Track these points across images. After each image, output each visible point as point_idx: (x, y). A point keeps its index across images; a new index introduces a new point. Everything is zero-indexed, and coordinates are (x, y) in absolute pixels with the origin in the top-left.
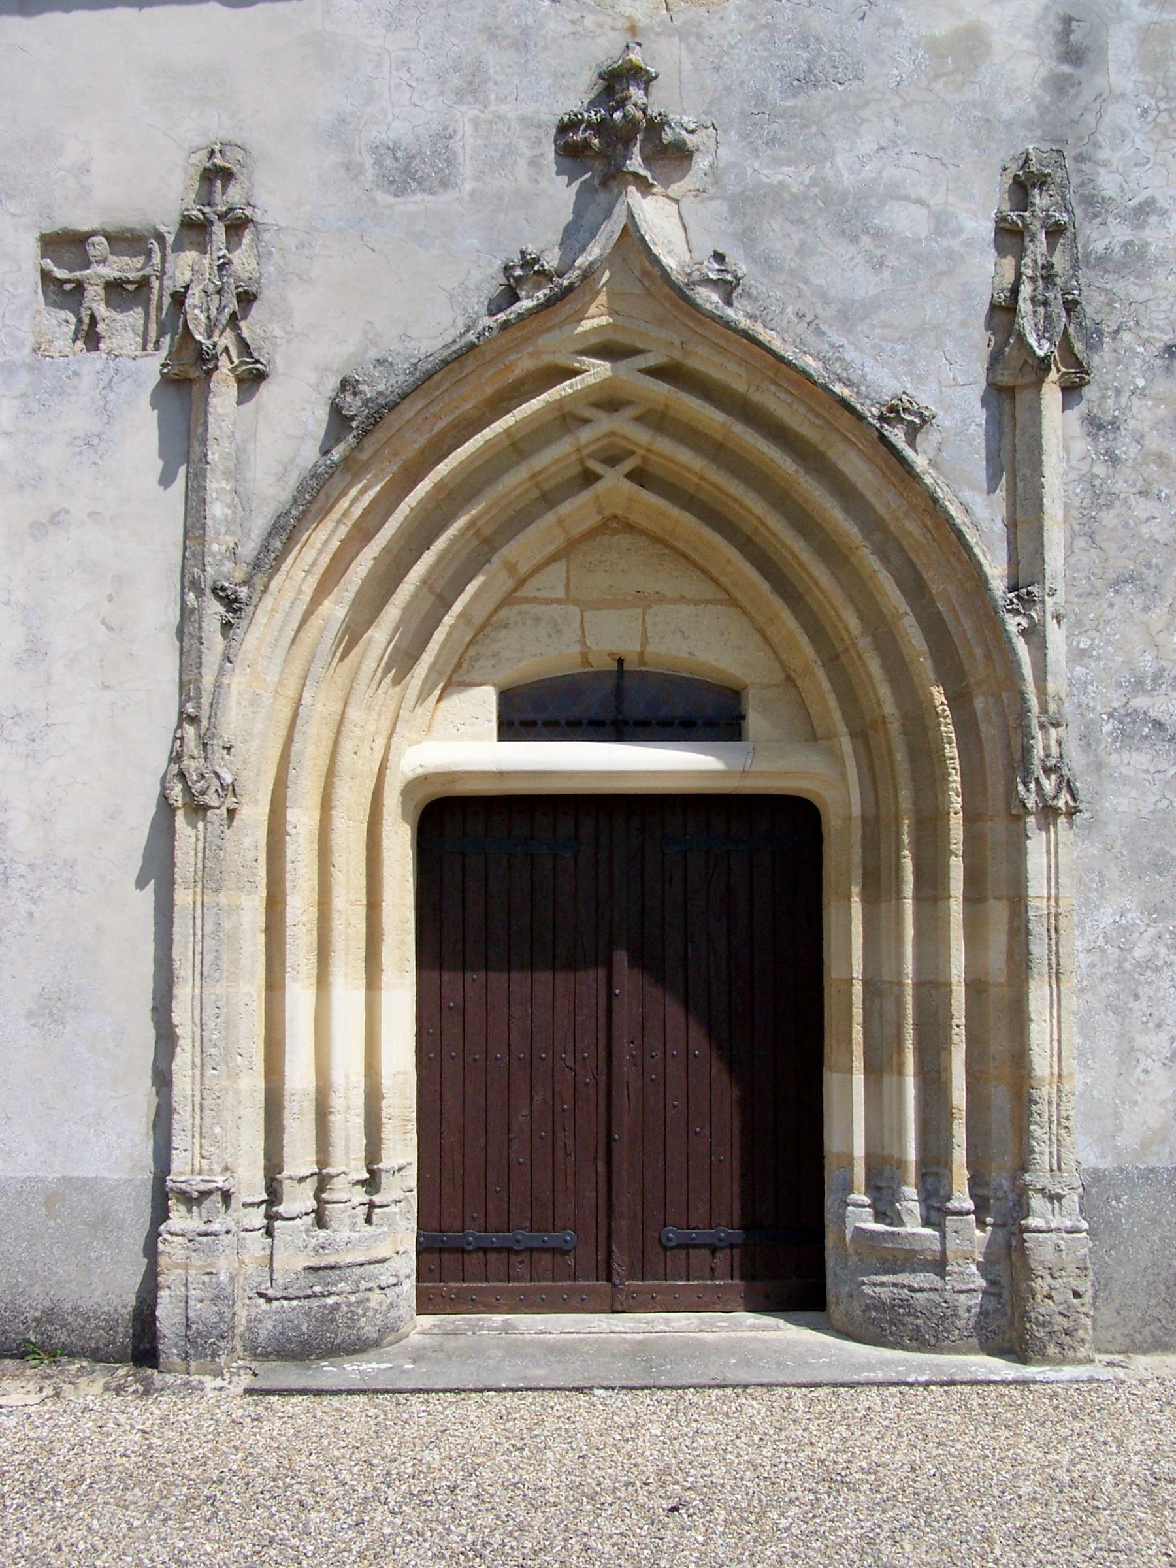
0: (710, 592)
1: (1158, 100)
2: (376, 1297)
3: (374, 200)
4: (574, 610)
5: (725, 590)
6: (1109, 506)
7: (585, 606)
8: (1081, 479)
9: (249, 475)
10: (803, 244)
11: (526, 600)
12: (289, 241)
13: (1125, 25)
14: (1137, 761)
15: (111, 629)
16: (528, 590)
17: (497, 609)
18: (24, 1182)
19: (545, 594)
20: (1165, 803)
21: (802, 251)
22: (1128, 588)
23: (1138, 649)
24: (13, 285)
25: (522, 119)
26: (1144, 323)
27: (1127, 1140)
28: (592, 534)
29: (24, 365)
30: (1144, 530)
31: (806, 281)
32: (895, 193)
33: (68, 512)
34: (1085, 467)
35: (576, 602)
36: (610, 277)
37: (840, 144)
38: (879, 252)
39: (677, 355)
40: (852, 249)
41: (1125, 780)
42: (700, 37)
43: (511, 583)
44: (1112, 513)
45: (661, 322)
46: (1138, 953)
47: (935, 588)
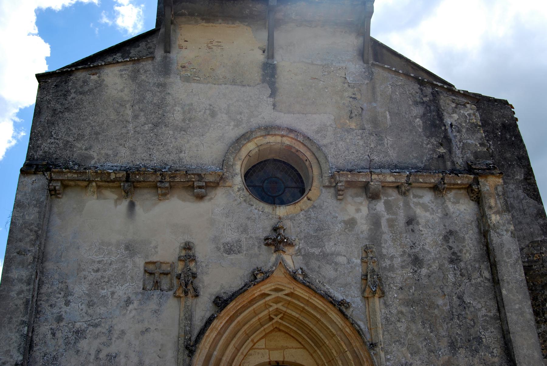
0: (299, 345)
1: (393, 234)
3: (223, 256)
5: (302, 345)
6: (391, 324)
7: (270, 350)
8: (384, 318)
9: (194, 320)
10: (319, 265)
12: (204, 265)
13: (384, 218)
15: (159, 357)
16: (256, 346)
17: (249, 351)
21: (319, 267)
22: (397, 343)
23: (401, 358)
24: (138, 274)
25: (256, 237)
26: (395, 282)
29: (140, 293)
30: (400, 329)
31: (321, 274)
32: (339, 254)
33: (150, 328)
35: (268, 349)
37: (326, 243)
38: (336, 267)
39: (292, 291)
40: (331, 267)
43: (252, 344)
44: (392, 325)
45: (289, 283)
47: (354, 344)
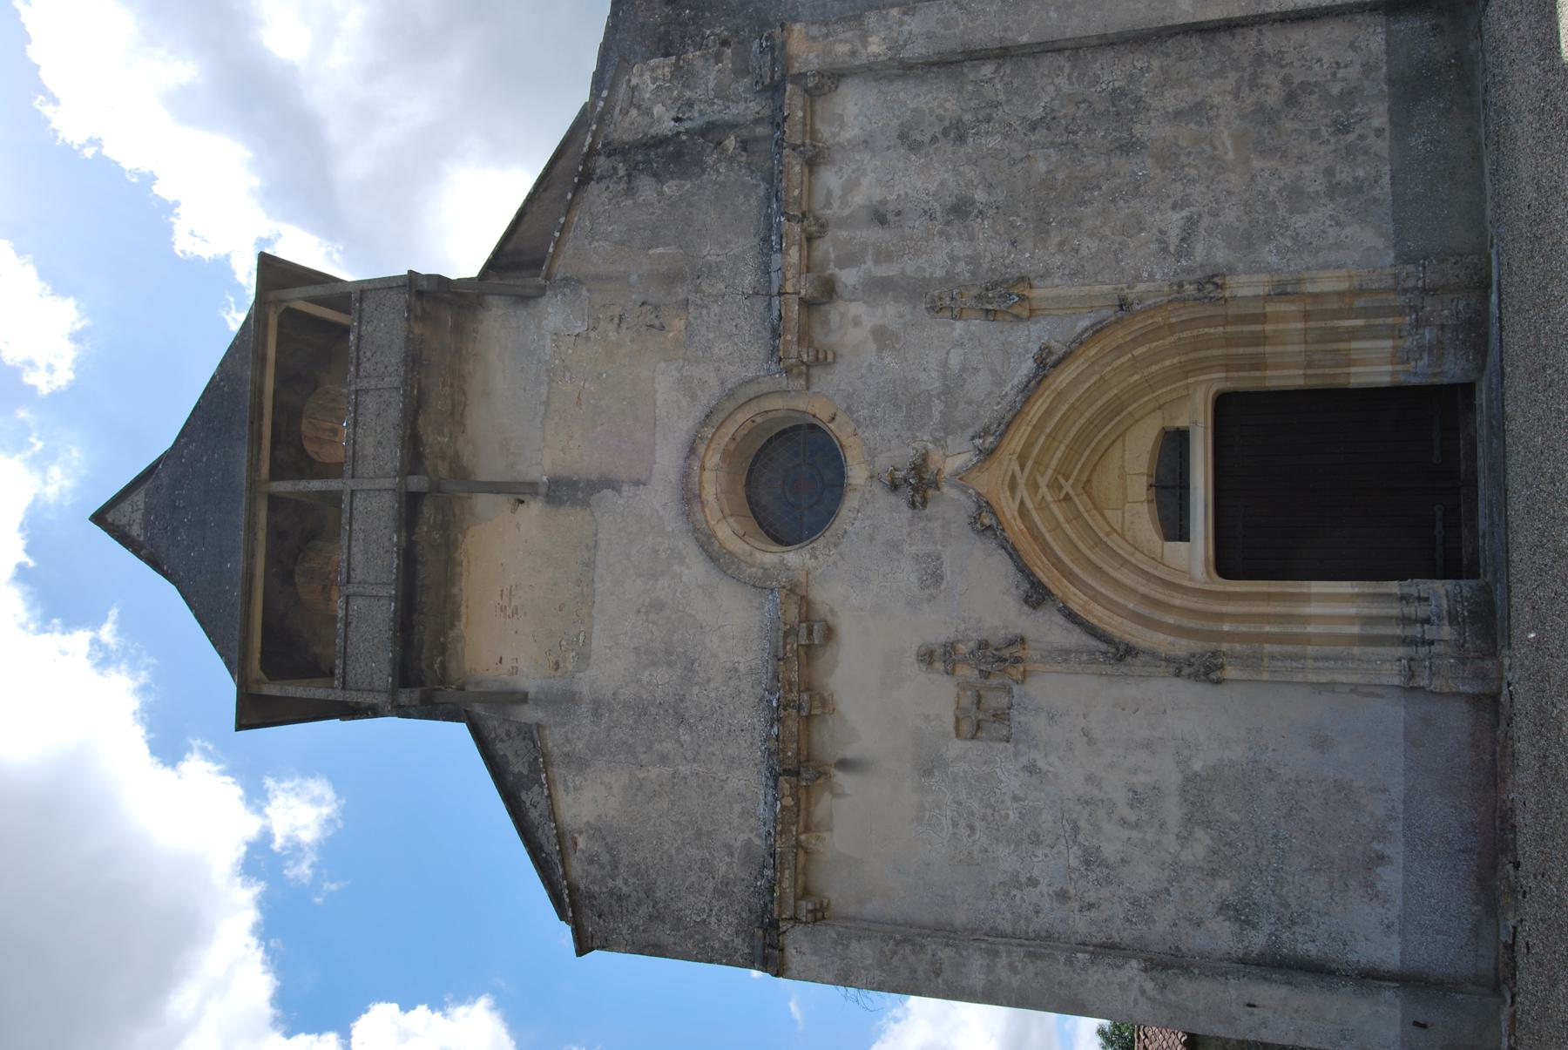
0: (1119, 444)
2: (1465, 593)
4: (1127, 506)
5: (1119, 437)
10: (966, 403)
11: (1123, 529)
12: (962, 627)
14: (1199, 250)
15: (1138, 710)
16: (1118, 527)
17: (1127, 541)
18: (1406, 758)
19: (1120, 519)
20: (1219, 236)
27: (1380, 243)
28: (1090, 497)
31: (983, 401)
32: (944, 364)
34: (1066, 278)
35: (1124, 505)
36: (1362, 327)
37: (923, 387)
38: (970, 370)
39: (1015, 457)
41: (1208, 254)
42: (875, 449)
46: (1289, 244)
47: (1121, 341)
